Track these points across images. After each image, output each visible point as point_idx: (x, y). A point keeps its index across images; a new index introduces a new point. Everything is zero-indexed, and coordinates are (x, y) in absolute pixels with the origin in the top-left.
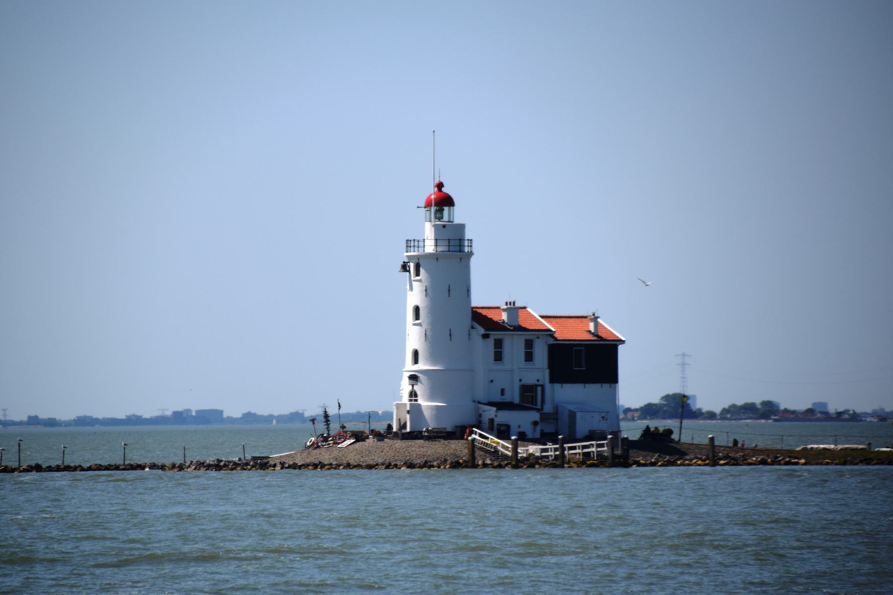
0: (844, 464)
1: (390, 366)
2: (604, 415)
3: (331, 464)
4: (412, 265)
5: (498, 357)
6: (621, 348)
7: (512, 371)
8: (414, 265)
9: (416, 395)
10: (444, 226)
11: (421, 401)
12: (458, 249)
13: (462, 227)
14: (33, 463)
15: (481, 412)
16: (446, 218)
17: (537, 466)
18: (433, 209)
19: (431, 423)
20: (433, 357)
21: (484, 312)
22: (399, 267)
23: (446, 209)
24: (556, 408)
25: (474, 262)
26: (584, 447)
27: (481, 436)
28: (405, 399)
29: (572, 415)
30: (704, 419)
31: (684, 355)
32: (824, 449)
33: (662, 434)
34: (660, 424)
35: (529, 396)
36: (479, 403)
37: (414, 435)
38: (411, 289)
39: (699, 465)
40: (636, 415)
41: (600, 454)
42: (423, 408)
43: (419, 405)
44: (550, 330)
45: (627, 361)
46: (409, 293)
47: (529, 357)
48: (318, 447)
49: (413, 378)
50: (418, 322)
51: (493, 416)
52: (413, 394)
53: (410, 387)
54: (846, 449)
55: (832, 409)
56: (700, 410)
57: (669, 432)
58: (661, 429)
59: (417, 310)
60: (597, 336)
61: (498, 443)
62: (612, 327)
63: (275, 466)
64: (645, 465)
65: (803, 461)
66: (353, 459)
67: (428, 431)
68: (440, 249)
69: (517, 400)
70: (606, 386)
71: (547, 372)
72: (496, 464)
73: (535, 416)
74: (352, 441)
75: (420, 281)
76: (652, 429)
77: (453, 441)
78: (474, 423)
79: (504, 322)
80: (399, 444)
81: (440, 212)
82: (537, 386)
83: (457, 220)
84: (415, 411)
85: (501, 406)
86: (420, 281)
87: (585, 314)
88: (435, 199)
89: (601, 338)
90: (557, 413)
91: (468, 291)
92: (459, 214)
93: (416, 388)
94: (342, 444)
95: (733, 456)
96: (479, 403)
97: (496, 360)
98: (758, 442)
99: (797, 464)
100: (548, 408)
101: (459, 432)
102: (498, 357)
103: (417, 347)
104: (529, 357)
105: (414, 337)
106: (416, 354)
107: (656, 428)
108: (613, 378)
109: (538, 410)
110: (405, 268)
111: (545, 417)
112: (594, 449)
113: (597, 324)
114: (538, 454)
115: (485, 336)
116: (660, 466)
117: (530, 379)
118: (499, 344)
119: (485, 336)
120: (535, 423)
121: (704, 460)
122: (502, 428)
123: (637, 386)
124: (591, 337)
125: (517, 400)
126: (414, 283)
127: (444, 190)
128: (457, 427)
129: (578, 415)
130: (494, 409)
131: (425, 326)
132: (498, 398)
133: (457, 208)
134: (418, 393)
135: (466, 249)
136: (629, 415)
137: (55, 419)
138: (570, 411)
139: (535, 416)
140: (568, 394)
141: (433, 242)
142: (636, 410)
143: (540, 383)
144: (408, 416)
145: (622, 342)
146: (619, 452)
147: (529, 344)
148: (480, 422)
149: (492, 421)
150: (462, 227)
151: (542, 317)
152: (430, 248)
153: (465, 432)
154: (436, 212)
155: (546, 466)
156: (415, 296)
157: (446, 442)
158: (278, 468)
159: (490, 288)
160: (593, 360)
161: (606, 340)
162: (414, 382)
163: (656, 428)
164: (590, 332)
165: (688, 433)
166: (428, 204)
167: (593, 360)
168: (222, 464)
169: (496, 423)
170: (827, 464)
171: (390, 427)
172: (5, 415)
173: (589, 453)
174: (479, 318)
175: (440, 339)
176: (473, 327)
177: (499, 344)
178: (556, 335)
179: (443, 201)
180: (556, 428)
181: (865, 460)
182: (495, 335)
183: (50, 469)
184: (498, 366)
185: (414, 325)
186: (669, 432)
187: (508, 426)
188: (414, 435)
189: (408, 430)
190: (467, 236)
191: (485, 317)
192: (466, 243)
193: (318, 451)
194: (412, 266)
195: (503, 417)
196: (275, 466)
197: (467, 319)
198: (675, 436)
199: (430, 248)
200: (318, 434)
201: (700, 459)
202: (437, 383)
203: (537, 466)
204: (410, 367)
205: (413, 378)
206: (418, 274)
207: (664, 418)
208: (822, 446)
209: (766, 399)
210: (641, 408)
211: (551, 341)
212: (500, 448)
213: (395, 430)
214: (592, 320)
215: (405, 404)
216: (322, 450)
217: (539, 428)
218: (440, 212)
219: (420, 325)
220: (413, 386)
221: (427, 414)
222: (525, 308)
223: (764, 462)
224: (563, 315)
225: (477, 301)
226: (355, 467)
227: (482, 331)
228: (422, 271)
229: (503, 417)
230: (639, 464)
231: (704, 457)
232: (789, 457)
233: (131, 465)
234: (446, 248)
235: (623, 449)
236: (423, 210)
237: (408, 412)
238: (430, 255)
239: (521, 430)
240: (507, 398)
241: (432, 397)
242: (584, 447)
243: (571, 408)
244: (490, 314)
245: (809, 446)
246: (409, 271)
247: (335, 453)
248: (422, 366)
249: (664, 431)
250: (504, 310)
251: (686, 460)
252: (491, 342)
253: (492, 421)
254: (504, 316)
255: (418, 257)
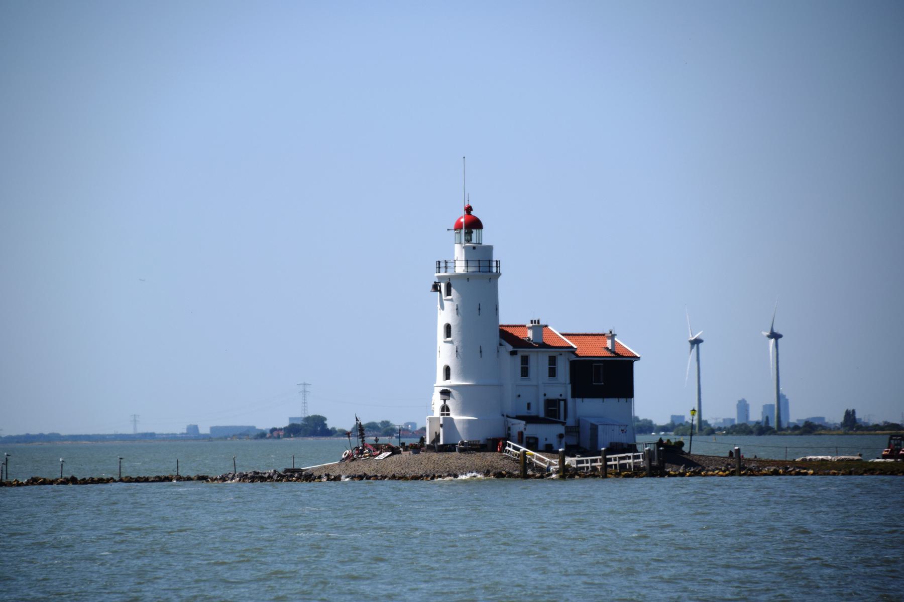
0: (850, 474)
1: (421, 379)
2: (623, 428)
3: (376, 476)
4: (443, 285)
5: (525, 373)
6: (636, 364)
7: (537, 386)
8: (445, 285)
9: (448, 410)
10: (474, 248)
11: (454, 415)
12: (487, 269)
13: (489, 249)
14: (69, 476)
15: (510, 425)
16: (474, 240)
17: (577, 477)
18: (463, 231)
19: (463, 436)
20: (465, 373)
21: (510, 330)
22: (431, 287)
23: (474, 231)
24: (578, 421)
25: (502, 283)
26: (621, 458)
27: (515, 448)
28: (437, 413)
29: (594, 429)
30: (338, 436)
31: (305, 384)
32: (822, 460)
33: (674, 446)
34: (673, 438)
35: (553, 411)
36: (508, 417)
37: (448, 448)
38: (442, 307)
39: (721, 476)
40: (281, 433)
41: (636, 466)
42: (455, 422)
43: (452, 419)
44: (572, 347)
45: (642, 377)
46: (439, 311)
47: (552, 373)
48: (354, 459)
49: (445, 393)
50: (449, 339)
51: (522, 429)
52: (445, 409)
53: (442, 402)
54: (843, 460)
55: (204, 430)
56: (333, 429)
57: (681, 444)
58: (673, 441)
59: (448, 328)
60: (614, 353)
61: (533, 455)
62: (627, 344)
63: (320, 477)
64: (675, 476)
65: (811, 472)
66: (392, 469)
67: (463, 443)
68: (470, 270)
69: (542, 414)
70: (623, 400)
71: (569, 386)
72: (538, 475)
73: (560, 429)
74: (389, 453)
75: (451, 300)
76: (665, 442)
77: (487, 454)
78: (503, 436)
79: (529, 339)
80: (435, 456)
81: (469, 233)
82: (560, 400)
83: (485, 242)
84: (448, 424)
85: (530, 420)
86: (451, 300)
87: (601, 332)
88: (465, 222)
89: (618, 355)
90: (579, 426)
91: (497, 309)
92: (487, 237)
93: (448, 402)
94: (302, 457)
95: (738, 466)
96: (508, 417)
97: (550, 376)
98: (759, 452)
99: (806, 474)
100: (570, 422)
101: (493, 445)
102: (525, 373)
103: (448, 364)
104: (552, 373)
105: (445, 353)
106: (447, 370)
107: (668, 440)
108: (628, 393)
109: (563, 424)
110: (436, 288)
111: (569, 430)
112: (631, 461)
113: (613, 342)
114: (575, 466)
115: (513, 353)
116: (690, 476)
117: (554, 394)
118: (525, 360)
119: (513, 353)
120: (561, 436)
121: (724, 471)
122: (531, 441)
123: (655, 400)
124: (608, 354)
125: (542, 414)
126: (445, 303)
127: (472, 213)
128: (488, 440)
129: (600, 428)
130: (524, 422)
131: (456, 343)
132: (524, 412)
133: (484, 231)
134: (450, 408)
135: (494, 270)
136: (275, 434)
137: (650, 422)
138: (592, 424)
139: (560, 429)
140: (589, 409)
141: (463, 263)
142: (281, 429)
143: (563, 397)
144: (441, 430)
145: (637, 358)
146: (655, 464)
147: (552, 361)
148: (509, 435)
149: (521, 434)
150: (489, 249)
151: (563, 335)
152: (460, 268)
153: (497, 444)
154: (466, 233)
155: (585, 477)
156: (446, 315)
157: (482, 454)
158: (324, 479)
159: (514, 310)
160: (610, 375)
161: (623, 356)
162: (446, 397)
163: (668, 440)
164: (607, 348)
165: (698, 447)
166: (458, 227)
167: (610, 375)
168: (266, 475)
169: (525, 436)
170: (834, 474)
171: (423, 440)
172: (135, 428)
173: (625, 464)
174: (506, 336)
175: (470, 356)
176: (501, 345)
177: (525, 360)
178: (577, 352)
179: (472, 224)
180: (580, 441)
181: (869, 470)
182: (522, 352)
183: (84, 482)
184: (525, 382)
185: (445, 342)
186: (681, 444)
187: (536, 439)
188: (448, 448)
189: (441, 443)
190: (495, 258)
191: (512, 334)
192: (494, 264)
193: (354, 462)
194: (443, 286)
195: (532, 430)
196: (320, 477)
197: (496, 338)
198: (685, 449)
199: (460, 268)
200: (353, 447)
201: (720, 470)
202: (469, 398)
203: (577, 477)
204: (441, 382)
205: (445, 393)
206: (449, 293)
207: (305, 436)
208: (820, 457)
209: (385, 419)
210: (285, 428)
211: (573, 358)
212: (534, 460)
213: (428, 443)
214: (609, 338)
215: (438, 418)
216: (360, 462)
217: (563, 441)
218: (469, 233)
219: (451, 342)
220: (445, 401)
221: (459, 427)
222: (546, 326)
223: (776, 473)
224: (581, 332)
225: (505, 319)
226: (400, 478)
227: (511, 348)
228: (453, 291)
229: (532, 430)
230: (670, 476)
231: (723, 468)
232: (798, 467)
233: (158, 477)
234: (476, 269)
235: (659, 460)
236: (454, 232)
237: (441, 426)
238: (460, 276)
239: (548, 442)
240: (533, 412)
241: (463, 412)
242: (621, 458)
243: (593, 421)
244: (517, 333)
245: (808, 458)
246: (440, 291)
247: (374, 465)
248: (454, 381)
249: (676, 443)
250: (530, 328)
251: (708, 470)
252: (518, 359)
253: (521, 434)
254: (530, 334)
255: (449, 278)
